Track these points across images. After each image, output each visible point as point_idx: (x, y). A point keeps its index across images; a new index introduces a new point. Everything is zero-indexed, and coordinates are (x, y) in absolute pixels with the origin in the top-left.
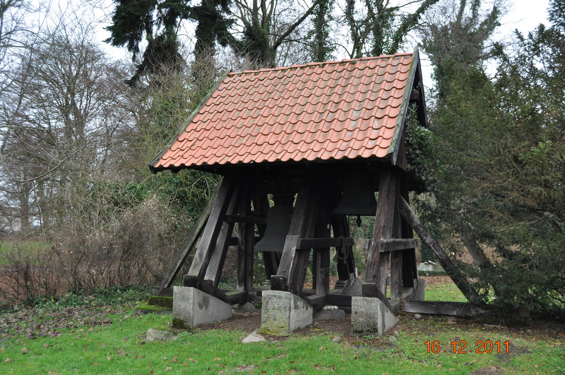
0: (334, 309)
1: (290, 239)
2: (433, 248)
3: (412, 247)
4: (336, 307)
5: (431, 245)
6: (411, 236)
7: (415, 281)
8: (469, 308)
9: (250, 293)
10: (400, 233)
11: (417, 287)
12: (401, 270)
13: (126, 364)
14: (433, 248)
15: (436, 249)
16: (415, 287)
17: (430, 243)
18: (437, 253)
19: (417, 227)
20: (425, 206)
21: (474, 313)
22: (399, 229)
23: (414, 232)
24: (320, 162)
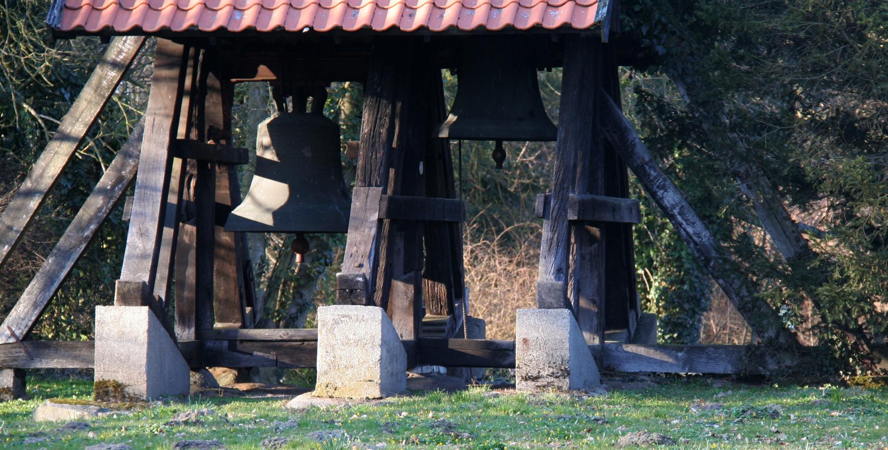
0: (439, 373)
1: (363, 196)
2: (679, 218)
3: (627, 220)
4: (443, 370)
5: (676, 212)
6: (625, 194)
7: (632, 316)
8: (762, 355)
9: (210, 344)
10: (601, 182)
11: (637, 330)
12: (603, 271)
13: (532, 233)
14: (679, 218)
15: (686, 220)
16: (633, 330)
17: (673, 207)
18: (690, 230)
19: (642, 166)
20: (738, 338)
21: (773, 366)
22: (600, 174)
23: (632, 178)
24: (455, 33)
